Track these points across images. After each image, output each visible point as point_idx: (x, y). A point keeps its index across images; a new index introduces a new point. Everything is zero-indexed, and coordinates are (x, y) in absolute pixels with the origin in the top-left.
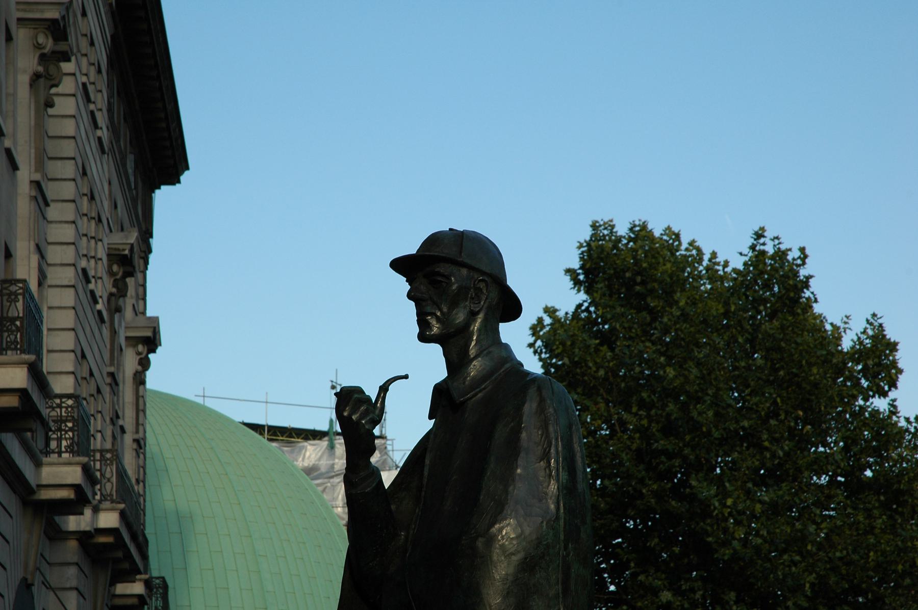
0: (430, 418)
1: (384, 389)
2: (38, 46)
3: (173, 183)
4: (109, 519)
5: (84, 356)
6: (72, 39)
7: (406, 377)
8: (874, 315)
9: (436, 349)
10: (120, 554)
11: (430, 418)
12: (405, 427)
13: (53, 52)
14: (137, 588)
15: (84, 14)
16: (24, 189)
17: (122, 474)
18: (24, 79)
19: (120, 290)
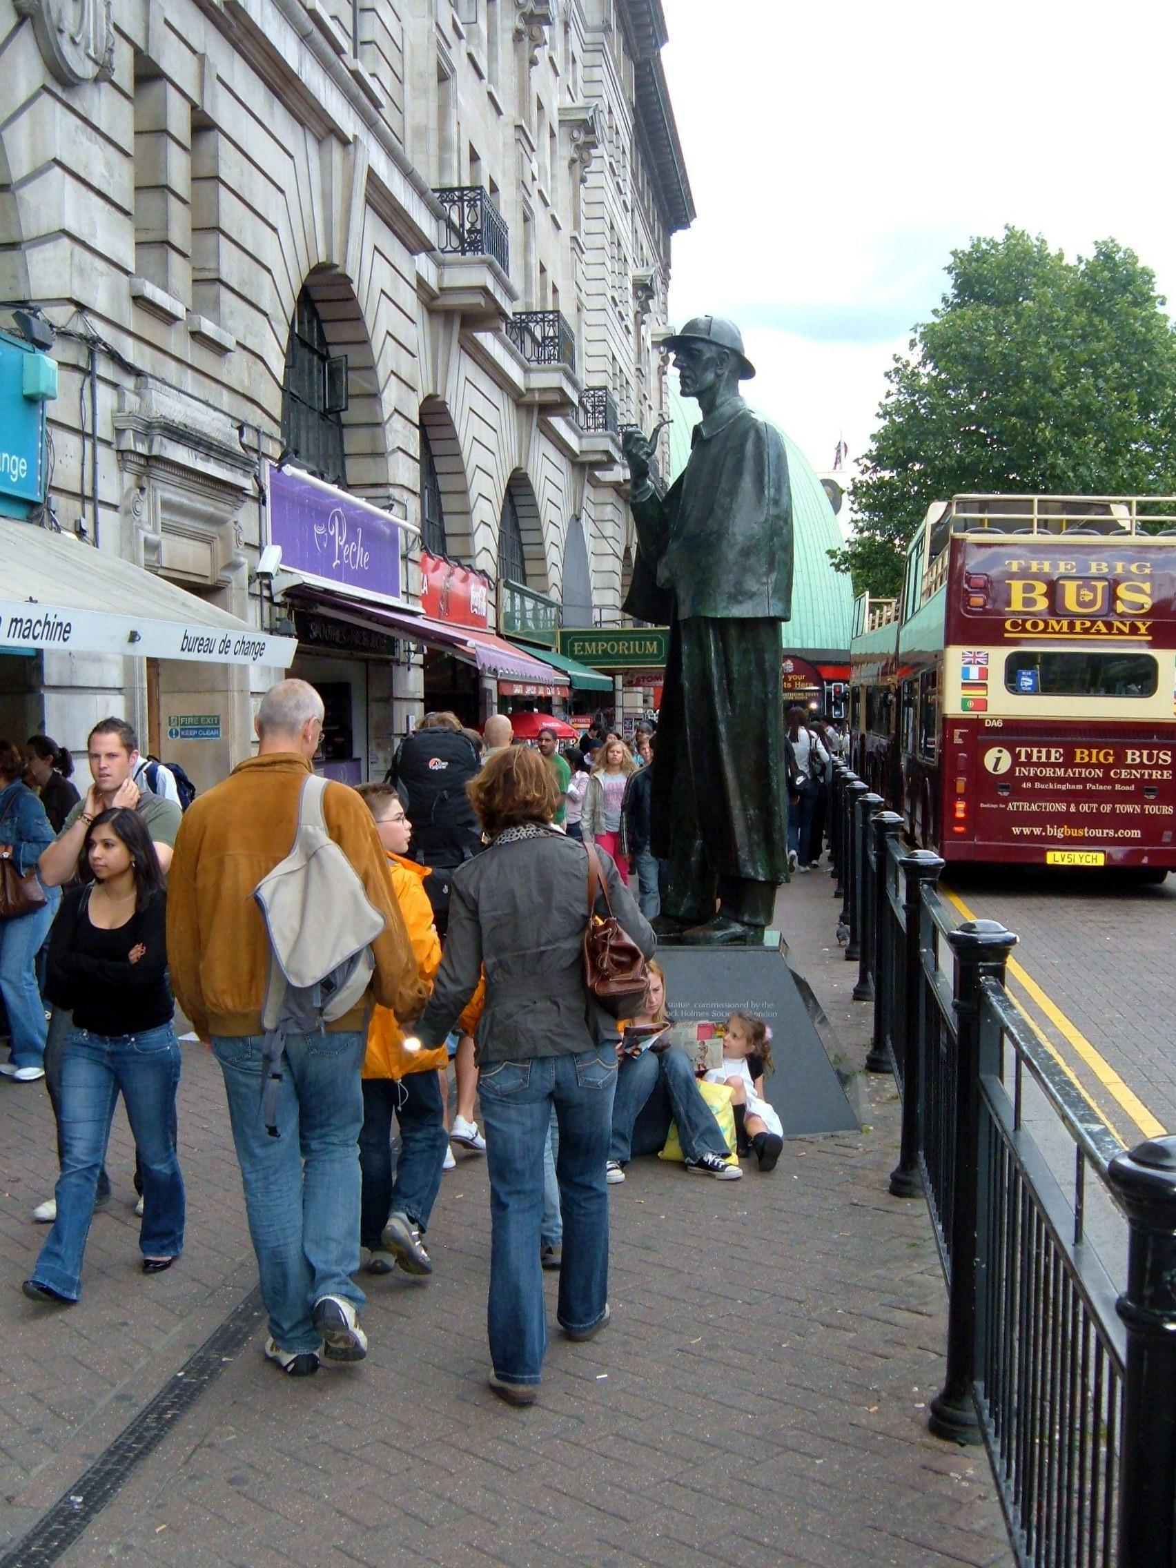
3: (685, 228)
5: (614, 358)
6: (598, 132)
9: (694, 401)
12: (675, 457)
13: (585, 143)
15: (610, 112)
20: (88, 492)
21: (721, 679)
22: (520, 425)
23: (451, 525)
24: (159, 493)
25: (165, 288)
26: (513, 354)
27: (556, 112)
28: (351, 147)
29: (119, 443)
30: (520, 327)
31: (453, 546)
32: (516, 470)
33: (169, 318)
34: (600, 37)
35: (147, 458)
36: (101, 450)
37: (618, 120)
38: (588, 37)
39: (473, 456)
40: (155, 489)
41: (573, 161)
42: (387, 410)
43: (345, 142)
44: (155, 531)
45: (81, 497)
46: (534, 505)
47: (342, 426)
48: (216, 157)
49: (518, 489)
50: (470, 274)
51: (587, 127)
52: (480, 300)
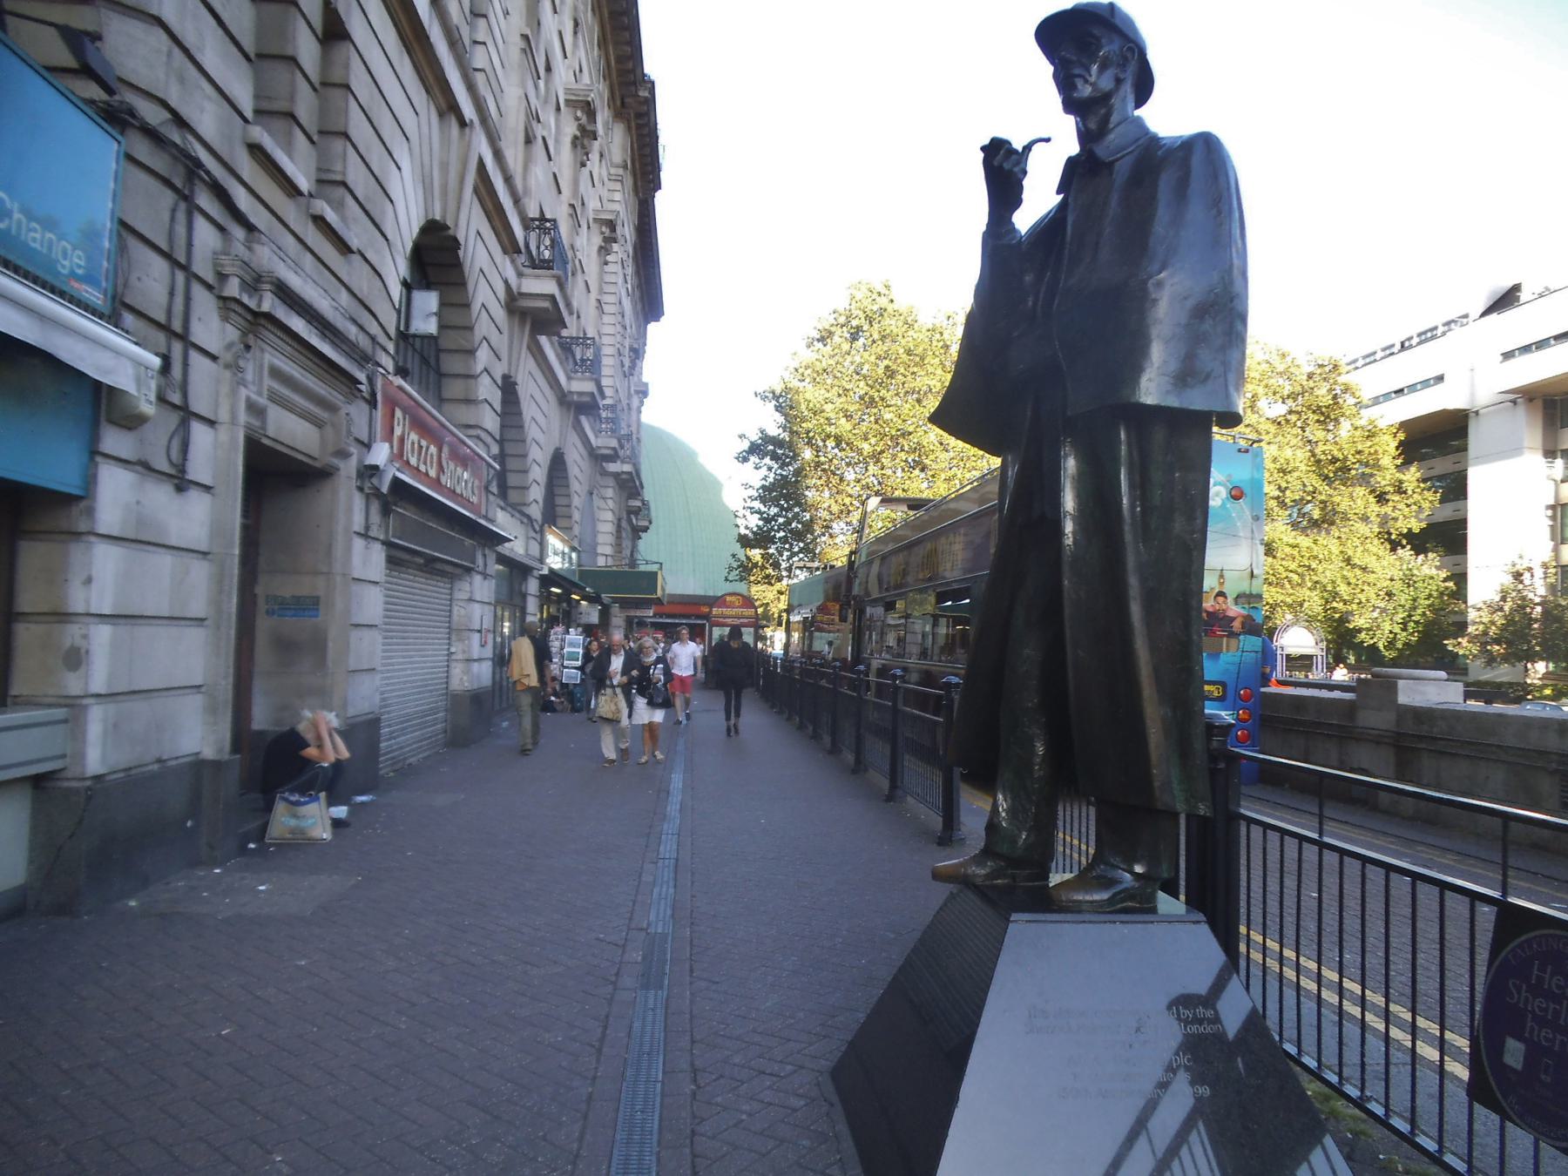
1: (1028, 148)
4: (627, 468)
7: (1048, 140)
12: (1039, 197)
14: (639, 504)
16: (593, 303)
18: (595, 248)
19: (633, 366)
20: (177, 326)
21: (1132, 506)
23: (512, 480)
24: (267, 357)
25: (291, 157)
28: (467, 130)
29: (221, 290)
30: (566, 348)
31: (513, 496)
33: (290, 188)
34: (621, 171)
35: (256, 314)
36: (198, 291)
37: (627, 231)
38: (613, 171)
39: (532, 431)
40: (262, 350)
42: (479, 368)
43: (463, 124)
44: (260, 394)
45: (165, 328)
46: (566, 478)
47: (441, 375)
48: (347, 66)
49: (558, 463)
50: (540, 285)
51: (611, 225)
52: (546, 304)
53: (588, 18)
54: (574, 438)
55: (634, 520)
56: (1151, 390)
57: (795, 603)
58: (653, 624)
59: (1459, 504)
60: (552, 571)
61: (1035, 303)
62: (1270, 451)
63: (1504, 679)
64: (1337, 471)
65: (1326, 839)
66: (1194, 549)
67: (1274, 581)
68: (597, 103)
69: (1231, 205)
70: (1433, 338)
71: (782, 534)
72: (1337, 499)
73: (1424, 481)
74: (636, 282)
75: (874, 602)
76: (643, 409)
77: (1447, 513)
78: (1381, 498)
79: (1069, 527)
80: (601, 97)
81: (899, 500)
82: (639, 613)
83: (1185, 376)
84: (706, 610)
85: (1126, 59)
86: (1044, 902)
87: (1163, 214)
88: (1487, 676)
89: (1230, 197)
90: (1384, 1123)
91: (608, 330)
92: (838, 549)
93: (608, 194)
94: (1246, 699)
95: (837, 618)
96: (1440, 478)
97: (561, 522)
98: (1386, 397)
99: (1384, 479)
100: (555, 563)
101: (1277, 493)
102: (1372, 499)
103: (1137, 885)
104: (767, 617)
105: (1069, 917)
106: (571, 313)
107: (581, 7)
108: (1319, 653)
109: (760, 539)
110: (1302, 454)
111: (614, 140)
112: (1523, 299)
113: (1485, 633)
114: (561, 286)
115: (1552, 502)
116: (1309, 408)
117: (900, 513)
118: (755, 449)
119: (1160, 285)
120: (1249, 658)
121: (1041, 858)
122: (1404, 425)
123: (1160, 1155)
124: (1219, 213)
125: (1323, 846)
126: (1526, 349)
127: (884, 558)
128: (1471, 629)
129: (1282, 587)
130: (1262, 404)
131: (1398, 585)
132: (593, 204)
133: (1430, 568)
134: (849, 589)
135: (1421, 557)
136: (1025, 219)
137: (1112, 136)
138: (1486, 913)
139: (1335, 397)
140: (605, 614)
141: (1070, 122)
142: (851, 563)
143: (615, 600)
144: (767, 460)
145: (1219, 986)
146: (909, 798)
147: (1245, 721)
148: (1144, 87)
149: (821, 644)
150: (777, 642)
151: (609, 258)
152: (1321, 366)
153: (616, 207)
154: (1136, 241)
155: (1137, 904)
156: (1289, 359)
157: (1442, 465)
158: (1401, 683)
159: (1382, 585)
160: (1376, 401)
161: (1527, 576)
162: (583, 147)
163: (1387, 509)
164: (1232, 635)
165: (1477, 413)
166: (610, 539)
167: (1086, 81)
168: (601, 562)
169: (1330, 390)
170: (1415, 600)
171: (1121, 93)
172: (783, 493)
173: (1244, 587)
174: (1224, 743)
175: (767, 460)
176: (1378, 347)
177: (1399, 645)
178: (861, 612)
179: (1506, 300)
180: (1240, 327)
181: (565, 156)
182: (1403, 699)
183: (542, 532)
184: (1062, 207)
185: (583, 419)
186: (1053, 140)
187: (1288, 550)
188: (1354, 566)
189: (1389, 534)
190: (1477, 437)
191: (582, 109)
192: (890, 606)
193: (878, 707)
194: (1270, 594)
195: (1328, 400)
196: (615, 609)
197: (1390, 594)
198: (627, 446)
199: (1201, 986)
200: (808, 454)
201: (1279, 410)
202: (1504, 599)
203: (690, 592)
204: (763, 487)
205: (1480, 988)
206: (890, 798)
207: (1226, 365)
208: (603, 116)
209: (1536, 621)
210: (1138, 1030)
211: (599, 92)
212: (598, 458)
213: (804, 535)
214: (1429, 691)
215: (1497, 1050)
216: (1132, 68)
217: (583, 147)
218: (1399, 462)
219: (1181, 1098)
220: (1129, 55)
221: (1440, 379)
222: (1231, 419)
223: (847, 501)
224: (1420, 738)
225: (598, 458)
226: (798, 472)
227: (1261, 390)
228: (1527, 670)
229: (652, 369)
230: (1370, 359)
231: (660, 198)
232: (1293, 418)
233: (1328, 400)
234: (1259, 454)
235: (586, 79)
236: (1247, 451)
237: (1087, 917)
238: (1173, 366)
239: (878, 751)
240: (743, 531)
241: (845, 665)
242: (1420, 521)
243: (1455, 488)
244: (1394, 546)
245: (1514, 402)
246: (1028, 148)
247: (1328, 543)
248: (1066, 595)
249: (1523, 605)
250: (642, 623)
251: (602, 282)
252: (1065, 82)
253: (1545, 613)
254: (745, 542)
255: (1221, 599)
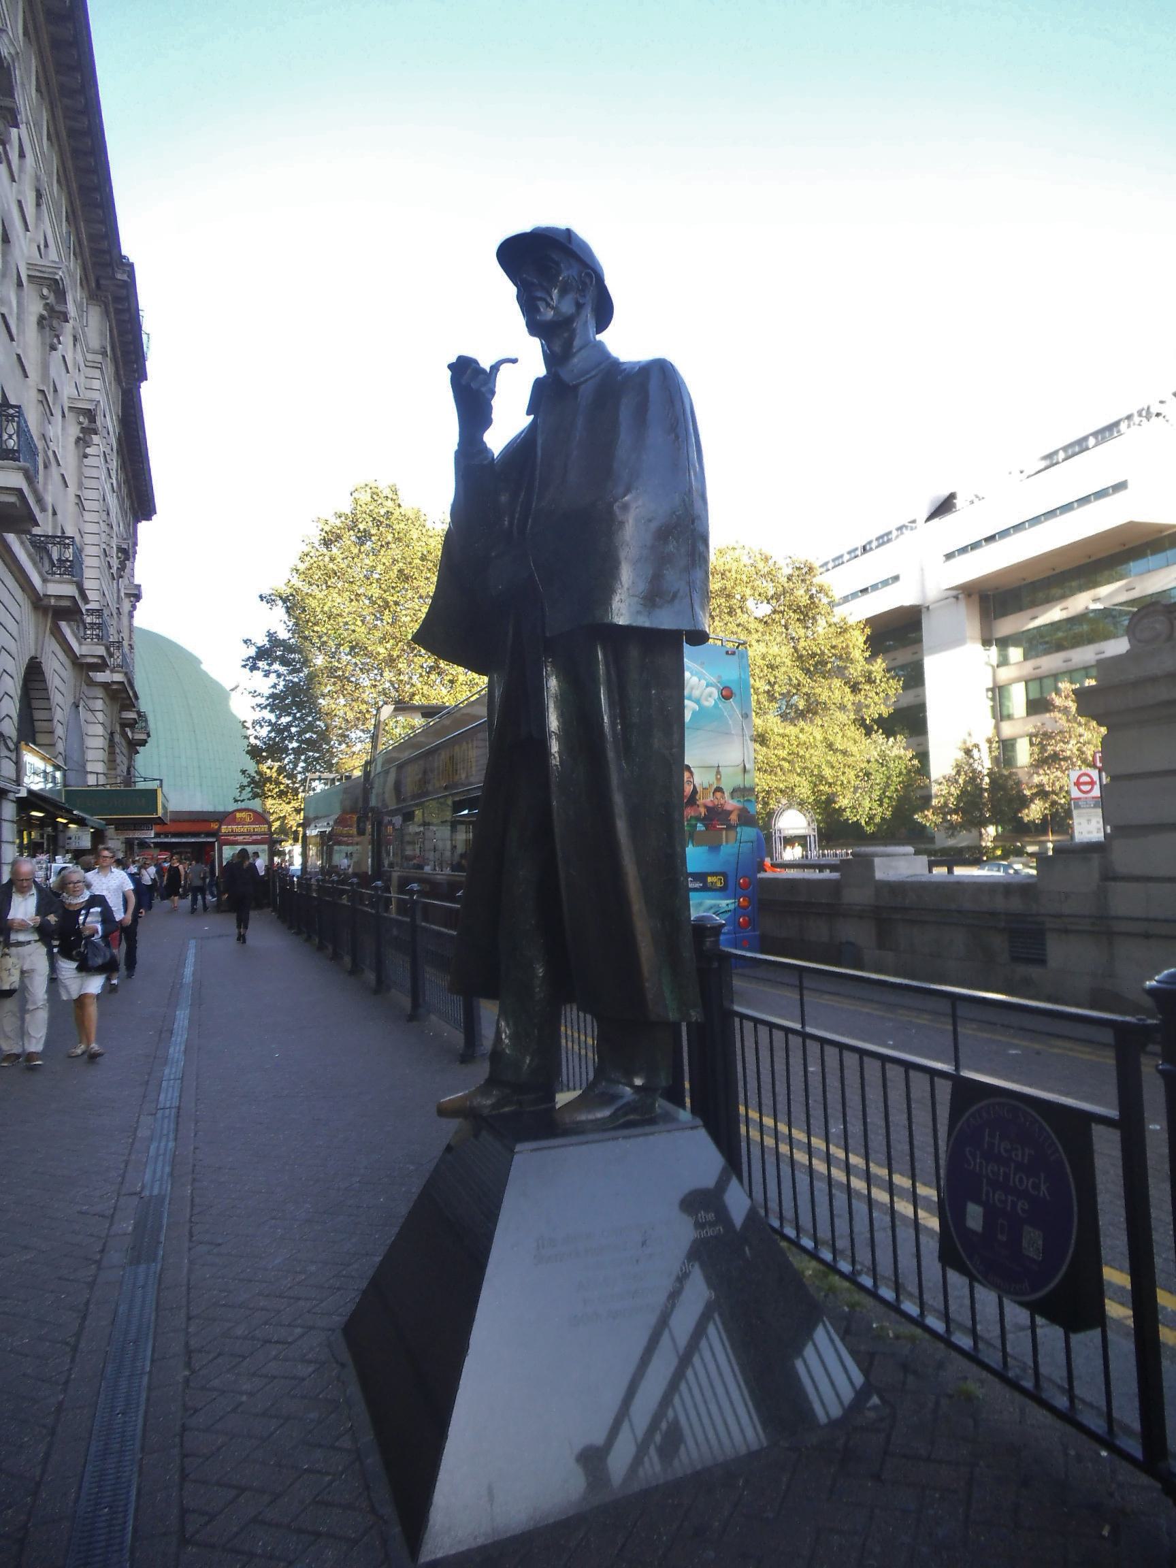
0: (528, 413)
1: (495, 368)
2: (80, 423)
4: (118, 677)
7: (514, 361)
8: (244, 666)
10: (124, 695)
11: (528, 413)
12: (509, 420)
14: (133, 715)
16: (72, 499)
17: (123, 655)
18: (72, 440)
19: (122, 568)
22: (37, 627)
26: (35, 564)
27: (66, 400)
30: (40, 547)
32: (33, 659)
34: (99, 358)
37: (109, 422)
38: (90, 357)
41: (79, 439)
51: (90, 415)
52: (12, 499)
53: (53, 190)
54: (53, 645)
55: (129, 731)
56: (623, 611)
57: (311, 816)
58: (157, 845)
59: (918, 690)
60: (30, 792)
61: (511, 524)
62: (755, 651)
63: (964, 844)
64: (815, 665)
65: (809, 1030)
66: (675, 764)
67: (768, 769)
68: (67, 282)
69: (687, 430)
70: (889, 541)
71: (295, 745)
72: (818, 691)
73: (888, 670)
74: (122, 477)
75: (393, 813)
76: (135, 613)
77: (909, 699)
78: (855, 688)
79: (555, 747)
80: (72, 276)
81: (414, 709)
82: (138, 835)
83: (653, 597)
84: (215, 826)
85: (584, 283)
86: (547, 1126)
87: (625, 436)
88: (951, 842)
89: (686, 420)
90: (873, 1293)
91: (90, 528)
92: (354, 757)
93: (84, 381)
94: (745, 887)
95: (354, 831)
96: (902, 667)
97: (41, 738)
98: (854, 595)
99: (855, 671)
100: (34, 783)
101: (767, 688)
102: (847, 690)
103: (636, 1097)
104: (284, 830)
105: (574, 1139)
106: (43, 510)
107: (44, 178)
108: (812, 833)
109: (274, 749)
110: (786, 650)
111: (88, 324)
112: (958, 507)
113: (946, 804)
114: (30, 478)
115: (991, 686)
116: (790, 607)
117: (418, 721)
118: (262, 654)
119: (625, 507)
120: (746, 848)
121: (547, 1078)
122: (870, 622)
123: (681, 1351)
124: (677, 437)
125: (805, 1036)
126: (963, 550)
127: (400, 767)
128: (934, 802)
129: (776, 774)
130: (750, 604)
131: (874, 766)
132: (67, 391)
133: (898, 749)
134: (366, 799)
135: (892, 739)
136: (497, 439)
137: (575, 360)
138: (944, 1090)
139: (811, 597)
140: (98, 837)
141: (535, 344)
142: (367, 774)
143: (109, 822)
144: (276, 666)
145: (721, 1185)
146: (433, 1018)
147: (745, 908)
148: (604, 312)
149: (341, 860)
150: (294, 857)
151: (88, 451)
152: (799, 569)
153: (96, 396)
154: (602, 467)
155: (637, 1118)
156: (771, 562)
157: (903, 656)
158: (877, 861)
159: (859, 768)
160: (846, 599)
161: (975, 753)
162: (52, 328)
163: (860, 697)
164: (730, 827)
165: (928, 608)
166: (101, 755)
167: (548, 305)
168: (91, 780)
169: (808, 590)
170: (888, 778)
171: (583, 317)
172: (295, 699)
173: (738, 781)
174: (717, 942)
175: (276, 666)
176: (844, 550)
177: (877, 820)
178: (379, 825)
179: (945, 507)
180: (702, 548)
181: (30, 337)
182: (879, 875)
183: (17, 750)
184: (533, 427)
185: (63, 624)
186: (520, 366)
187: (779, 739)
188: (835, 751)
189: (864, 720)
190: (930, 628)
191: (49, 287)
192: (408, 817)
193: (400, 924)
194: (761, 782)
195: (805, 601)
196: (111, 831)
197: (868, 774)
198: (117, 654)
199: (709, 1181)
200: (319, 661)
201: (764, 610)
202: (958, 773)
203: (197, 807)
204: (273, 696)
205: (942, 1162)
206: (413, 1017)
207: (690, 585)
208: (74, 298)
209: (986, 790)
210: (644, 1243)
211: (69, 270)
212: (82, 667)
213: (317, 747)
214: (901, 865)
215: (960, 1215)
216: (591, 293)
217: (52, 328)
218: (867, 654)
219: (698, 1293)
220: (588, 281)
221: (896, 578)
222: (699, 638)
223: (364, 707)
224: (899, 909)
225: (82, 667)
226: (311, 677)
227: (748, 592)
228: (981, 835)
229: (143, 570)
230: (838, 561)
231: (145, 388)
232: (777, 617)
233: (805, 601)
234: (744, 656)
235: (53, 254)
236: (733, 653)
237: (590, 1137)
238: (642, 587)
239: (398, 966)
240: (253, 741)
241: (365, 880)
242: (888, 706)
243: (914, 677)
244: (868, 732)
245: (956, 597)
246: (495, 368)
247: (812, 731)
248: (555, 815)
249: (974, 778)
250: (143, 844)
251: (81, 476)
252: (528, 303)
253: (992, 782)
254: (254, 752)
255: (718, 794)
